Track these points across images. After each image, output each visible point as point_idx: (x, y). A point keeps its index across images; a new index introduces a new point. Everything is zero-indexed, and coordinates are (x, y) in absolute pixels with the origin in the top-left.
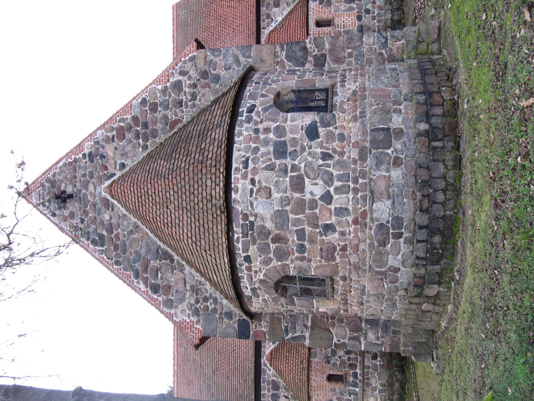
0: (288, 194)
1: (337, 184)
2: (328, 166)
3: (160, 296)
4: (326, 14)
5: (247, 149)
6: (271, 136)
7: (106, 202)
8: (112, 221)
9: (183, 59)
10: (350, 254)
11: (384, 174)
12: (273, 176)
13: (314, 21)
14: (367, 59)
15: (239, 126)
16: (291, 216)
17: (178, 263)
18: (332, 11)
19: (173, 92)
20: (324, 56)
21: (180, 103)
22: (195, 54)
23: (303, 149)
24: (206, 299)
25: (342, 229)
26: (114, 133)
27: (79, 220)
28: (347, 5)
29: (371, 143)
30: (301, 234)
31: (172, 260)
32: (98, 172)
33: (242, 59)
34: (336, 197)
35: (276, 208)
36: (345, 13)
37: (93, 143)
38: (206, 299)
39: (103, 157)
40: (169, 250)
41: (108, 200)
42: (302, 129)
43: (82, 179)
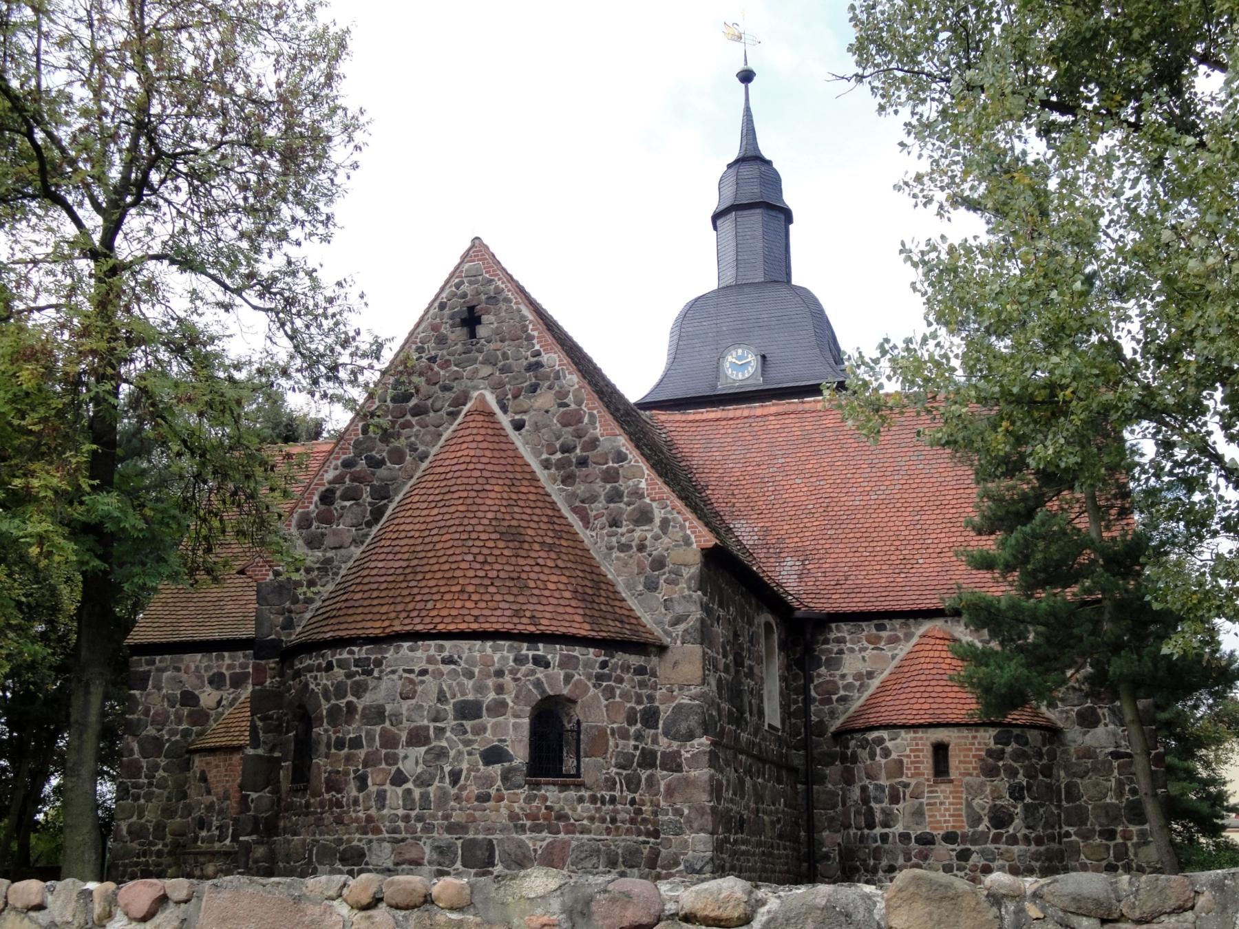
0: (405, 724)
1: (417, 793)
2: (442, 779)
3: (316, 507)
4: (962, 766)
6: (492, 695)
7: (461, 401)
8: (432, 414)
9: (687, 524)
10: (332, 813)
11: (427, 857)
12: (430, 702)
13: (946, 740)
14: (670, 840)
15: (511, 646)
16: (378, 729)
17: (367, 535)
18: (968, 778)
19: (634, 510)
20: (679, 768)
21: (615, 523)
22: (695, 546)
23: (467, 743)
25: (361, 799)
26: (573, 406)
27: (433, 353)
28: (986, 811)
29: (471, 840)
30: (356, 743)
31: (369, 525)
32: (509, 383)
34: (400, 791)
35: (388, 707)
36: (963, 807)
37: (557, 368)
39: (534, 388)
40: (384, 519)
41: (464, 404)
42: (500, 741)
43: (499, 353)
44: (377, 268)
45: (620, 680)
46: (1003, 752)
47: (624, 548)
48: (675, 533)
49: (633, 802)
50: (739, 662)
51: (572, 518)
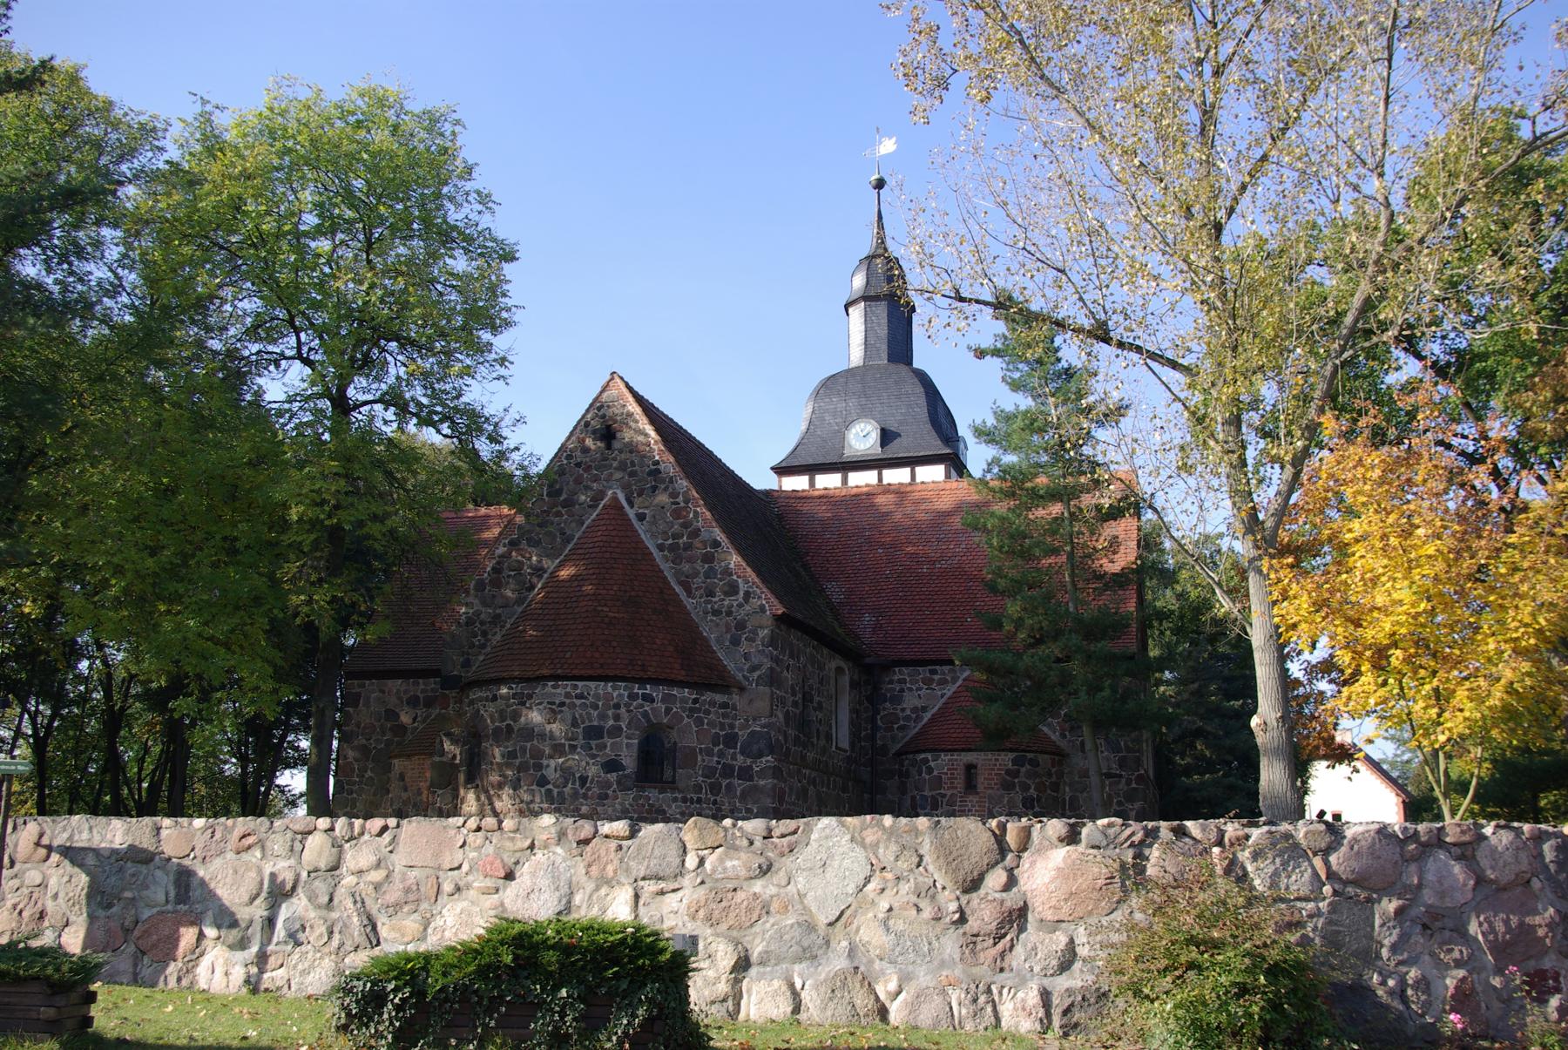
1: (556, 791)
5: (597, 696)
6: (611, 722)
21: (711, 594)
24: (485, 634)
33: (757, 674)
38: (485, 634)
39: (654, 489)
44: (532, 408)
45: (708, 712)
46: (1018, 771)
47: (716, 613)
48: (755, 603)
49: (715, 802)
50: (807, 698)
51: (678, 589)
